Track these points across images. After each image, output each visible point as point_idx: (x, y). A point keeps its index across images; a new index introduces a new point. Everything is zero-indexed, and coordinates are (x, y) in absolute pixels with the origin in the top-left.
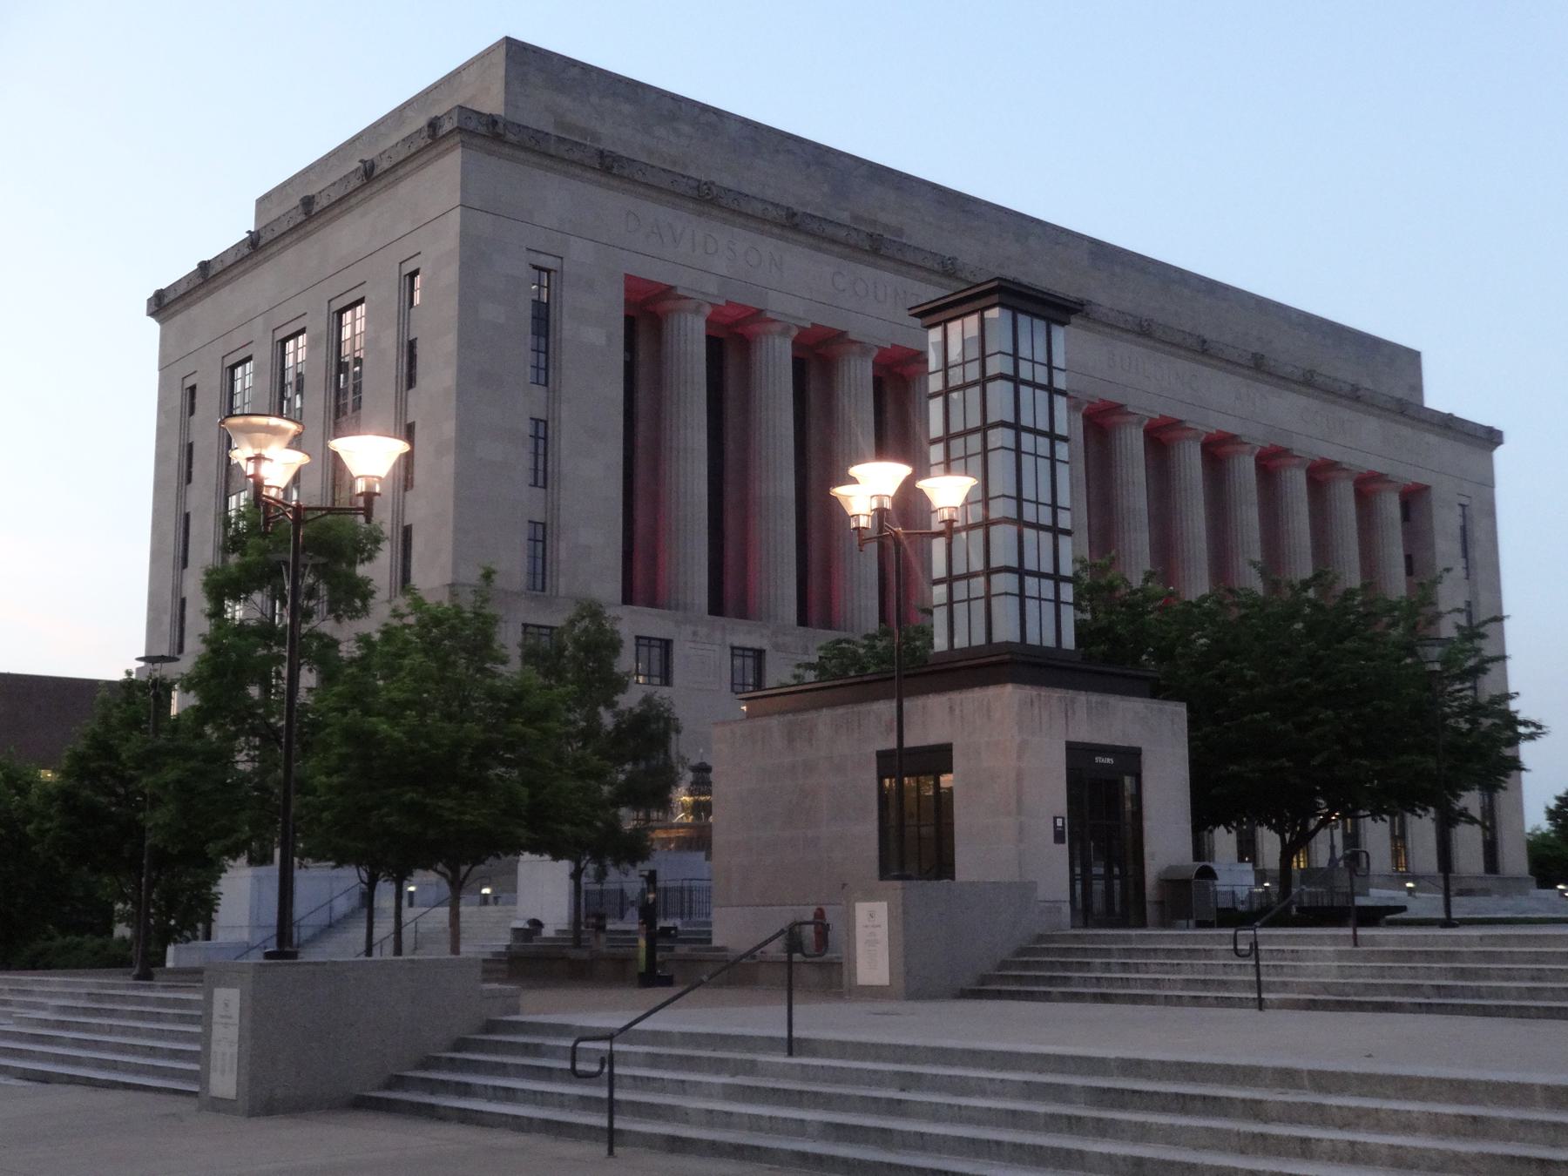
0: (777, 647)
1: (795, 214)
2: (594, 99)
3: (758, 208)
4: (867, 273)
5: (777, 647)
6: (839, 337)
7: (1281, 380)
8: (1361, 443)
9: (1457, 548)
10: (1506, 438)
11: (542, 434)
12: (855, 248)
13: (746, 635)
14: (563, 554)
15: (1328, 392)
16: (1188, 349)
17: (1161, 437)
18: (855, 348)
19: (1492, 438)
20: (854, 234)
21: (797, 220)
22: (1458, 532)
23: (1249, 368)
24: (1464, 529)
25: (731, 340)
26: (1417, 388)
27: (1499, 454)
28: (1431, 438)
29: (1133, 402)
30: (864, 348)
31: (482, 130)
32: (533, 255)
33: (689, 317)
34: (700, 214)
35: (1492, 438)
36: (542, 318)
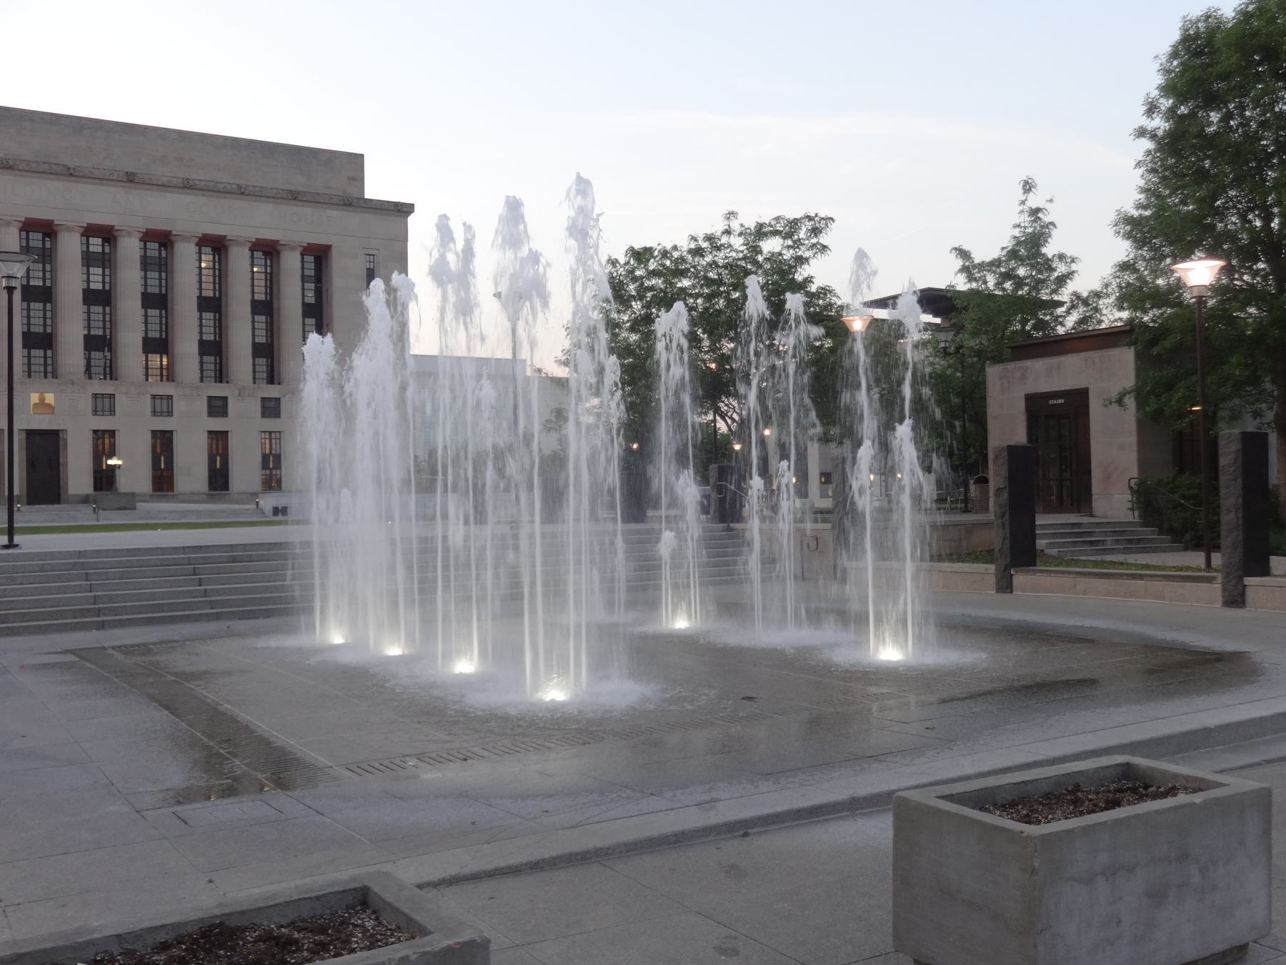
19: (403, 210)
28: (335, 214)
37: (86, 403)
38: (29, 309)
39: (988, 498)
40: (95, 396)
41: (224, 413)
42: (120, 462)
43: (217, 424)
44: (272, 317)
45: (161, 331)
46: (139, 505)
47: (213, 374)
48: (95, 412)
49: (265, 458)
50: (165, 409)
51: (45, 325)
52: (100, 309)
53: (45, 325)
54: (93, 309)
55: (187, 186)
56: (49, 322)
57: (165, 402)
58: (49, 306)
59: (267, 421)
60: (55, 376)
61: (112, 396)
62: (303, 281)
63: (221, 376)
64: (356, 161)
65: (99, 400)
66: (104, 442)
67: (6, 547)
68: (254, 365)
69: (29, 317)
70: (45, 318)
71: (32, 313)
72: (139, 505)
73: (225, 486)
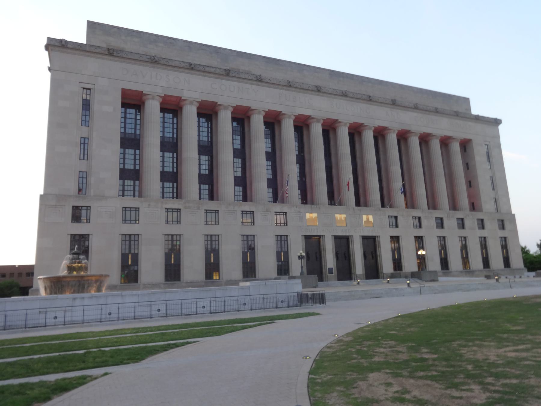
0: (185, 208)
1: (191, 64)
3: (177, 64)
4: (225, 82)
6: (336, 121)
7: (405, 108)
8: (440, 127)
9: (485, 158)
10: (503, 121)
11: (85, 142)
12: (219, 74)
13: (416, 213)
15: (426, 111)
16: (364, 100)
17: (425, 140)
18: (315, 120)
19: (497, 122)
20: (218, 70)
21: (193, 66)
23: (391, 104)
24: (488, 153)
25: (329, 129)
26: (469, 109)
27: (500, 127)
29: (413, 129)
30: (226, 108)
31: (57, 44)
32: (484, 150)
34: (154, 67)
35: (497, 122)
36: (86, 105)
38: (124, 154)
39: (254, 322)
42: (424, 253)
44: (212, 157)
45: (173, 167)
47: (207, 196)
48: (125, 221)
49: (124, 257)
50: (133, 218)
51: (135, 164)
52: (132, 151)
53: (135, 164)
54: (166, 154)
56: (137, 162)
58: (138, 152)
59: (76, 225)
60: (140, 196)
61: (217, 212)
63: (177, 195)
65: (128, 213)
68: (200, 189)
69: (124, 159)
71: (127, 156)
73: (136, 280)
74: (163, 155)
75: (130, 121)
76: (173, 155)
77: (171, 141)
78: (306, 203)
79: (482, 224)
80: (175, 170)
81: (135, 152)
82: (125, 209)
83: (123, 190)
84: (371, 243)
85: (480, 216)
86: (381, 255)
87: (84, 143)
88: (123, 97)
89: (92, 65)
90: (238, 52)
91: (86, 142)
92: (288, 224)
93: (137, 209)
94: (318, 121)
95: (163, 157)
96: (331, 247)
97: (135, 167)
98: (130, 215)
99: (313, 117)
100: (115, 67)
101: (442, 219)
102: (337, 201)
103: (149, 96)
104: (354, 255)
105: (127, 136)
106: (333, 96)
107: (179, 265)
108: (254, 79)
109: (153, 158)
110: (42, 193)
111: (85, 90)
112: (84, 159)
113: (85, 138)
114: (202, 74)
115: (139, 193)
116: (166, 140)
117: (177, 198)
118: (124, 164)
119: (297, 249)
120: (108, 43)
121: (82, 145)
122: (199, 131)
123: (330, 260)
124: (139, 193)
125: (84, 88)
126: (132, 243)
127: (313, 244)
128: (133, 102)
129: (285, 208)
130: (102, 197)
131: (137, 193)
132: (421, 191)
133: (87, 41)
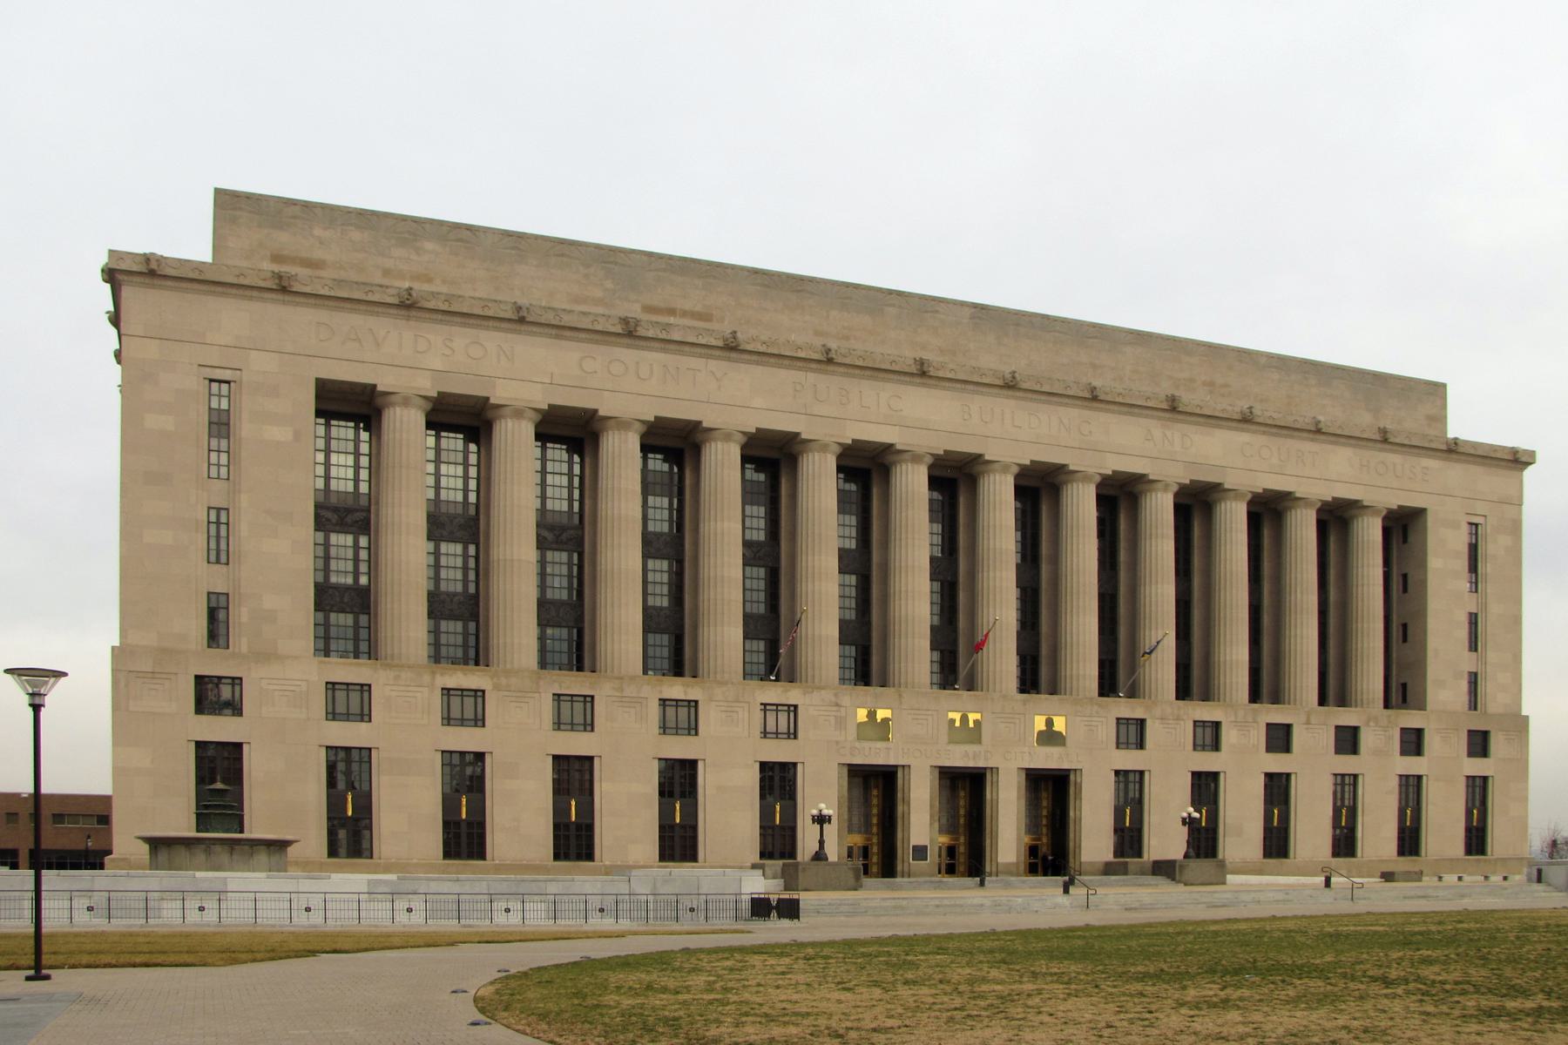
0: (497, 687)
2: (317, 232)
5: (497, 687)
14: (244, 619)
22: (1464, 550)
24: (1473, 550)
26: (1440, 419)
27: (1528, 473)
28: (1432, 463)
32: (1461, 540)
33: (510, 424)
34: (408, 318)
36: (220, 425)
37: (1108, 732)
40: (558, 697)
41: (1286, 747)
43: (1277, 763)
46: (1229, 877)
51: (356, 574)
53: (356, 574)
55: (1246, 420)
56: (363, 568)
57: (469, 702)
62: (646, 492)
64: (1436, 391)
66: (1130, 787)
67: (761, 908)
70: (356, 560)
72: (1229, 877)
74: (437, 548)
75: (342, 459)
76: (465, 549)
77: (460, 510)
78: (867, 684)
79: (1413, 742)
80: (472, 589)
81: (356, 542)
82: (332, 686)
83: (327, 638)
84: (1051, 791)
85: (1411, 719)
86: (1078, 821)
87: (218, 523)
88: (318, 397)
89: (231, 321)
90: (671, 257)
91: (223, 519)
92: (800, 734)
93: (365, 689)
94: (916, 458)
95: (437, 554)
96: (927, 797)
97: (356, 579)
98: (349, 702)
99: (899, 447)
100: (299, 321)
101: (1217, 725)
102: (222, 641)
103: (392, 398)
104: (995, 818)
105: (334, 500)
106: (971, 387)
107: (482, 825)
108: (714, 343)
109: (408, 561)
110: (117, 644)
111: (215, 386)
112: (218, 561)
113: (219, 510)
114: (554, 332)
115: (365, 645)
116: (444, 510)
117: (477, 664)
118: (326, 570)
119: (821, 795)
120: (276, 250)
121: (213, 527)
122: (543, 485)
123: (921, 821)
124: (365, 645)
125: (211, 381)
126: (355, 767)
127: (876, 787)
128: (350, 405)
129: (792, 695)
130: (267, 656)
131: (364, 647)
132: (1234, 653)
133: (217, 249)
